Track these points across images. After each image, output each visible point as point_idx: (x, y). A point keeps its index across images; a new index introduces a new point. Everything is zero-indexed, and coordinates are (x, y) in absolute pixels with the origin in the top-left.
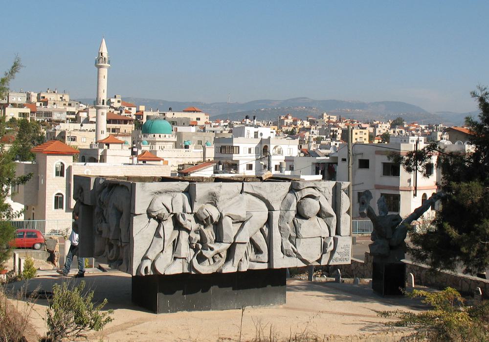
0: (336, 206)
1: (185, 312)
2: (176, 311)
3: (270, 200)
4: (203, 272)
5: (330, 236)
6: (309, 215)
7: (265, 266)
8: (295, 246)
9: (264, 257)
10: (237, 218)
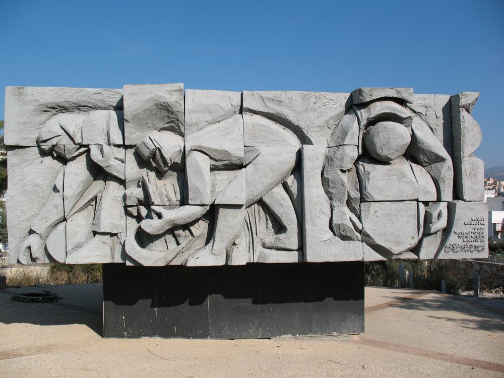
0: (452, 142)
1: (157, 340)
2: (139, 336)
3: (302, 124)
4: (146, 263)
5: (439, 200)
6: (384, 152)
7: (292, 258)
8: (359, 218)
9: (291, 238)
10: (222, 156)
